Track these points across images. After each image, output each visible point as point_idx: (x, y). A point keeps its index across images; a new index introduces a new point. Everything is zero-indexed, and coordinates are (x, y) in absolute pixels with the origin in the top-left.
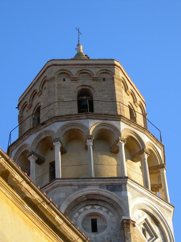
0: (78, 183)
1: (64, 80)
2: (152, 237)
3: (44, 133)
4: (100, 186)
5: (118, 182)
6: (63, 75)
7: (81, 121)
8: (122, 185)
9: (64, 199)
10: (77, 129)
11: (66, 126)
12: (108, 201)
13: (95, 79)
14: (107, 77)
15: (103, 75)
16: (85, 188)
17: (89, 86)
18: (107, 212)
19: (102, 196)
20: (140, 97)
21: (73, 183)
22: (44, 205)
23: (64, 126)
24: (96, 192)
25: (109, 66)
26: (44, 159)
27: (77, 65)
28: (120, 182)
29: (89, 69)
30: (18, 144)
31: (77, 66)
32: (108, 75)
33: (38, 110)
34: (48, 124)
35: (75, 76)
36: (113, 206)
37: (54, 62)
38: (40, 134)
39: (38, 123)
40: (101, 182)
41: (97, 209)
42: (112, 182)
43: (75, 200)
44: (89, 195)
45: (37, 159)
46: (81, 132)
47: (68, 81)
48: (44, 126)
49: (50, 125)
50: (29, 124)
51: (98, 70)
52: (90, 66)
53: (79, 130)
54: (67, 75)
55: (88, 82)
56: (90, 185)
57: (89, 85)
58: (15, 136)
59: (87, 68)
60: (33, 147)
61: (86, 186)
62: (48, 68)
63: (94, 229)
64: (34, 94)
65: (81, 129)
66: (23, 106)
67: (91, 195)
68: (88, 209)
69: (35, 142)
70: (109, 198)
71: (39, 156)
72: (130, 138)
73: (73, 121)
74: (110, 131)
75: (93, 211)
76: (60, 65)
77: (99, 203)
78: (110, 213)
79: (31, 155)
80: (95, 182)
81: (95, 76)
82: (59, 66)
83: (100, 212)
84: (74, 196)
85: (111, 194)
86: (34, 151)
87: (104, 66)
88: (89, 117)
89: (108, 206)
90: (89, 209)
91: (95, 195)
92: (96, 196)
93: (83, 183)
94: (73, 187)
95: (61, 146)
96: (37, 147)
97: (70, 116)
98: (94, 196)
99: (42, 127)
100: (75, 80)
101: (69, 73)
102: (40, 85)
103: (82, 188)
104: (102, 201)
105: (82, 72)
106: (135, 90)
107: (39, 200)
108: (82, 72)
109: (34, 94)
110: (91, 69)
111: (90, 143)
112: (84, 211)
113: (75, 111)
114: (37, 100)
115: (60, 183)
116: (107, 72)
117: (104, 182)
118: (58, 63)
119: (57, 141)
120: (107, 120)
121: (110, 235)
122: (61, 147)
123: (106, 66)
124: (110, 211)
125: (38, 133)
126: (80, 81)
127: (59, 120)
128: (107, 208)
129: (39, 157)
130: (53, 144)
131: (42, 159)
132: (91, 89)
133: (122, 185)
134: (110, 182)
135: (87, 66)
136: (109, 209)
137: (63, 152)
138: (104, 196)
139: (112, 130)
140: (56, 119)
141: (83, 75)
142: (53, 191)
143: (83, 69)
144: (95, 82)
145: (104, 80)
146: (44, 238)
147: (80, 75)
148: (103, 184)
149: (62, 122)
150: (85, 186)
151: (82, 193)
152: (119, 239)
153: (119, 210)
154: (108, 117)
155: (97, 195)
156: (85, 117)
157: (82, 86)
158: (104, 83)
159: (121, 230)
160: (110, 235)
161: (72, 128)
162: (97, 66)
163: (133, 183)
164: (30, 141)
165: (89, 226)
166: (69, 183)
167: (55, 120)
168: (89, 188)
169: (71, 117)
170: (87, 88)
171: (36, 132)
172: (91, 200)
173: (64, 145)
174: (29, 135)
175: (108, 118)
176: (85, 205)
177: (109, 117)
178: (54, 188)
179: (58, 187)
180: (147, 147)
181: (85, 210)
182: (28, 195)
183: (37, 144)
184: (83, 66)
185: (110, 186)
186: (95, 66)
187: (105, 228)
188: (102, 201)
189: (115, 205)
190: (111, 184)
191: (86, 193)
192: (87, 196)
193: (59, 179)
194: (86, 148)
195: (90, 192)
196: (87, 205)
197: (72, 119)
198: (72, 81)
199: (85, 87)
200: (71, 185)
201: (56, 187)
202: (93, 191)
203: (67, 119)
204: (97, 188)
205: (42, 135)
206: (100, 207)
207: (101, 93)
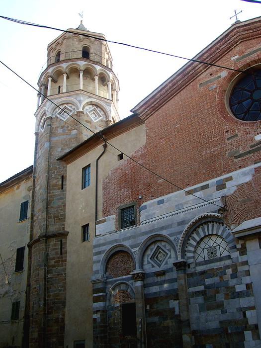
11: (103, 70)
33: (59, 54)
39: (58, 61)
43: (246, 247)
50: (53, 61)
58: (45, 67)
64: (57, 44)
66: (50, 48)
72: (101, 74)
109: (57, 44)
111: (97, 78)
113: (81, 56)
114: (58, 48)
121: (207, 321)
137: (68, 78)
145: (211, 74)
160: (207, 321)
161: (228, 109)
164: (50, 70)
180: (111, 79)
182: (129, 235)
194: (94, 80)
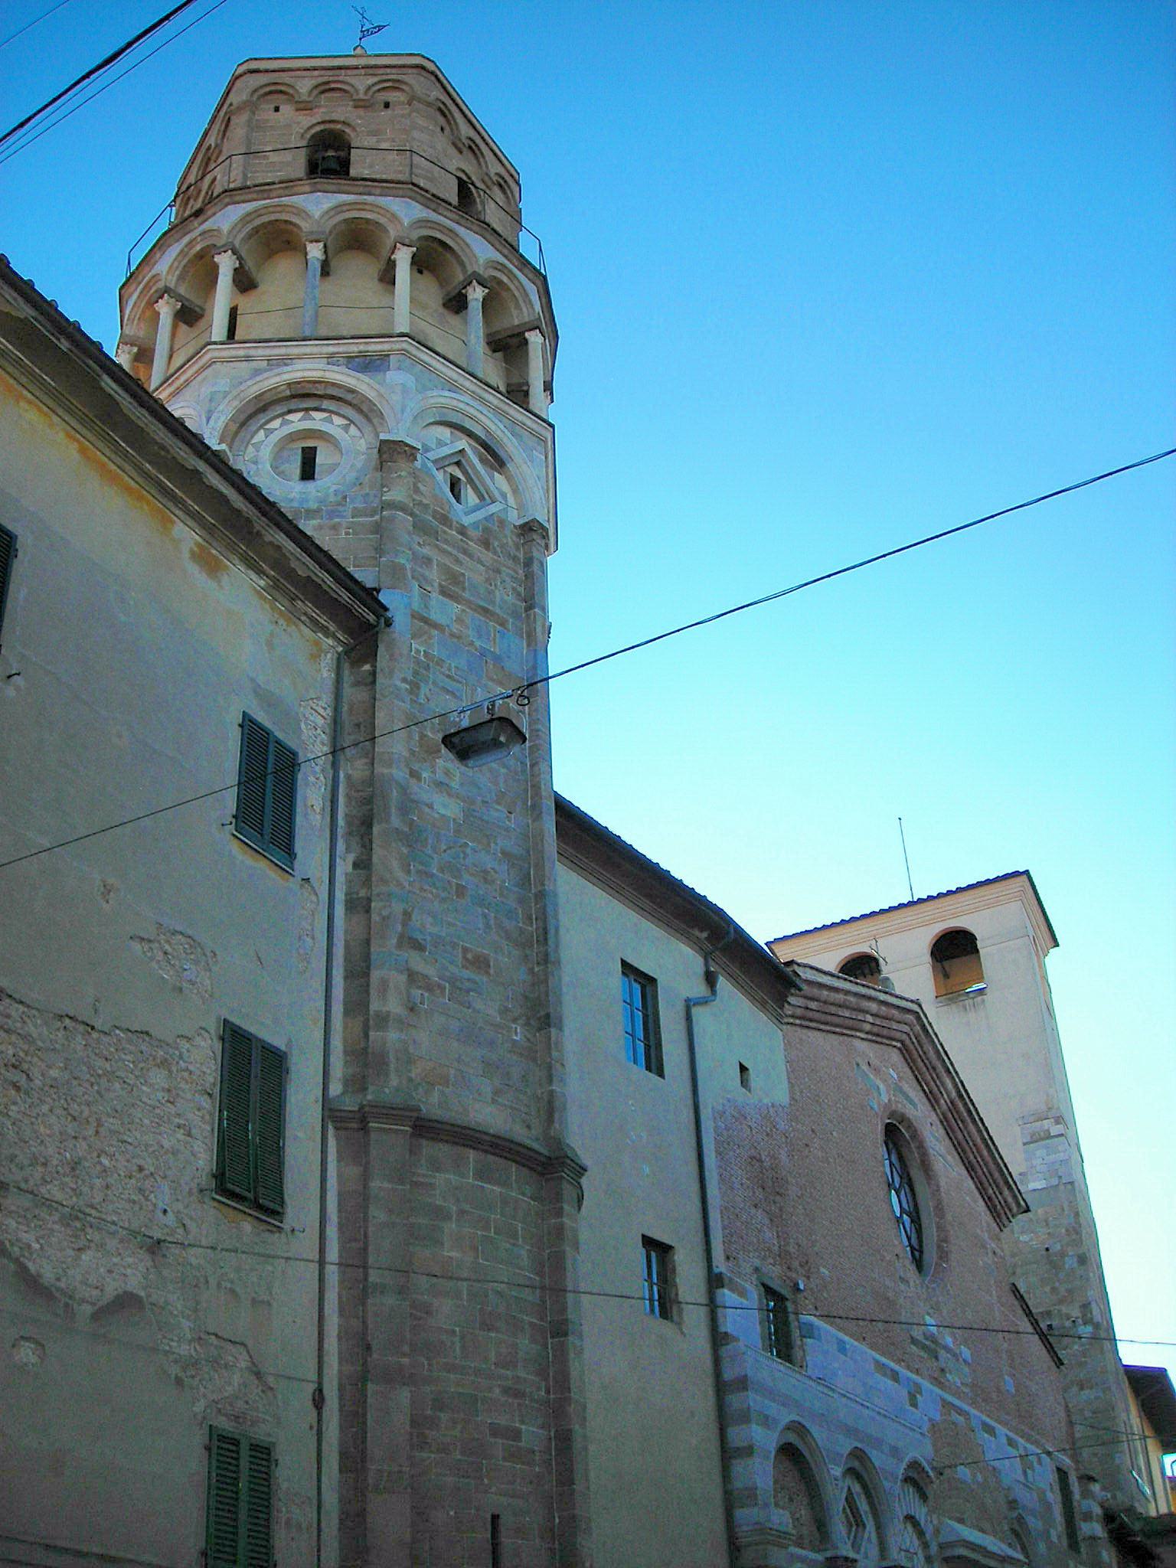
0: (268, 352)
1: (277, 109)
2: (481, 497)
3: (199, 239)
4: (330, 360)
5: (379, 347)
6: (276, 96)
7: (294, 199)
8: (391, 357)
9: (226, 394)
10: (286, 221)
11: (257, 213)
12: (349, 397)
13: (361, 105)
14: (395, 99)
15: (382, 93)
16: (286, 365)
17: (344, 123)
18: (346, 428)
19: (333, 384)
20: (501, 161)
21: (252, 352)
22: (59, 340)
23: (248, 214)
24: (315, 375)
25: (404, 70)
26: (203, 310)
27: (315, 69)
28: (386, 347)
29: (348, 79)
30: (141, 277)
31: (316, 73)
32: (397, 94)
34: (210, 213)
35: (305, 98)
36: (360, 411)
37: (254, 65)
38: (190, 242)
40: (331, 349)
41: (317, 421)
42: (362, 348)
44: (299, 383)
45: (179, 307)
46: (295, 230)
47: (287, 110)
48: (201, 219)
49: (214, 214)
51: (371, 81)
52: (349, 72)
53: (291, 223)
54: (285, 97)
55: (339, 111)
56: (299, 357)
57: (342, 120)
59: (342, 75)
60: (170, 277)
61: (289, 361)
62: (238, 81)
63: (308, 472)
65: (298, 222)
67: (303, 384)
68: (293, 422)
69: (176, 264)
70: (352, 391)
71: (187, 300)
73: (277, 200)
74: (377, 223)
75: (308, 425)
76: (267, 71)
77: (326, 404)
78: (353, 430)
79: (161, 297)
80: (315, 350)
81: (361, 96)
82: (266, 74)
83: (325, 427)
84: (254, 389)
85: (358, 379)
86: (172, 286)
87: (388, 70)
88: (319, 187)
89: (349, 412)
90: (297, 422)
91: (315, 382)
92: (317, 385)
93: (283, 351)
94: (254, 364)
95: (237, 265)
96: (181, 278)
97: (267, 187)
98: (311, 386)
99: (196, 224)
100: (304, 107)
101: (291, 91)
102: (219, 130)
103: (278, 365)
104: (332, 397)
105: (325, 88)
106: (487, 144)
107: (39, 322)
108: (325, 88)
110: (352, 81)
112: (282, 425)
115: (217, 354)
116: (397, 85)
117: (341, 349)
118: (262, 65)
119: (225, 252)
120: (369, 194)
122: (235, 270)
123: (394, 71)
124: (354, 423)
125: (186, 239)
126: (322, 110)
127: (237, 198)
128: (344, 417)
129: (186, 303)
130: (215, 260)
131: (197, 309)
132: (347, 130)
133: (388, 355)
134: (356, 349)
135: (343, 71)
136: (349, 419)
138: (339, 386)
139: (382, 220)
140: (230, 196)
141: (328, 95)
142: (199, 378)
143: (331, 79)
144: (361, 112)
145: (387, 105)
146: (62, 435)
147: (323, 96)
148: (337, 353)
149: (244, 205)
150: (285, 360)
151: (277, 379)
152: (368, 494)
153: (375, 421)
154: (373, 186)
155: (320, 382)
156: (307, 188)
157: (323, 122)
158: (385, 114)
159: (376, 469)
162: (371, 71)
163: (423, 351)
165: (295, 467)
166: (242, 353)
167: (227, 200)
168: (299, 365)
169: (271, 190)
170: (339, 126)
171: (181, 238)
172: (304, 395)
173: (250, 264)
174: (164, 248)
175: (373, 191)
176: (286, 410)
177: (376, 187)
178: (204, 368)
179: (214, 366)
181: (284, 423)
183: (180, 269)
184: (330, 73)
185: (357, 360)
186: (363, 71)
187: (332, 468)
188: (332, 397)
189: (365, 408)
190: (360, 352)
191: (286, 377)
192: (292, 386)
193: (215, 343)
195: (299, 374)
196: (290, 412)
197: (274, 194)
198: (297, 110)
199: (332, 126)
200: (248, 359)
201: (209, 366)
202: (306, 374)
203: (260, 196)
204: (322, 364)
205: (194, 243)
206: (325, 415)
207: (375, 139)
